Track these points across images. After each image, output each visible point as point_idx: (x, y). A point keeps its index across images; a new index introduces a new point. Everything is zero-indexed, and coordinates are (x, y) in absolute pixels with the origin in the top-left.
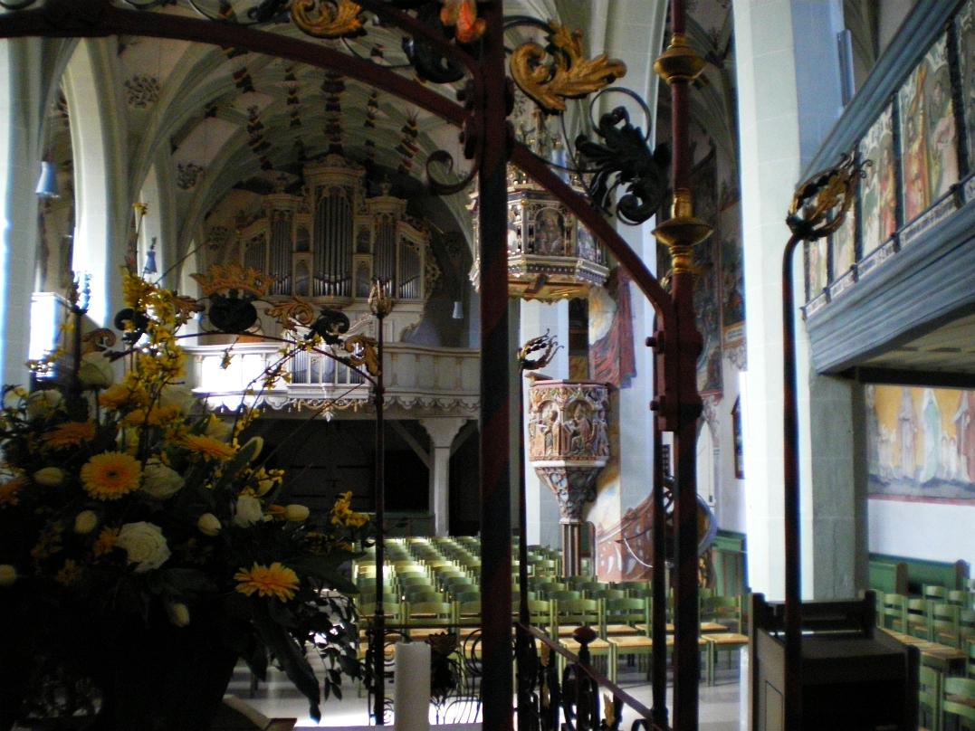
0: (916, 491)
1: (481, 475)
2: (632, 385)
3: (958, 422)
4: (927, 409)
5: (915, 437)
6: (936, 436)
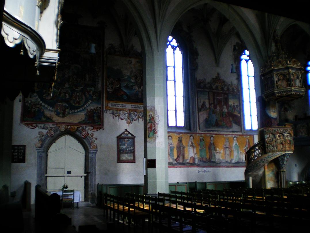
0: (231, 165)
1: (287, 152)
2: (105, 126)
3: (245, 149)
4: (235, 146)
5: (230, 152)
6: (238, 152)
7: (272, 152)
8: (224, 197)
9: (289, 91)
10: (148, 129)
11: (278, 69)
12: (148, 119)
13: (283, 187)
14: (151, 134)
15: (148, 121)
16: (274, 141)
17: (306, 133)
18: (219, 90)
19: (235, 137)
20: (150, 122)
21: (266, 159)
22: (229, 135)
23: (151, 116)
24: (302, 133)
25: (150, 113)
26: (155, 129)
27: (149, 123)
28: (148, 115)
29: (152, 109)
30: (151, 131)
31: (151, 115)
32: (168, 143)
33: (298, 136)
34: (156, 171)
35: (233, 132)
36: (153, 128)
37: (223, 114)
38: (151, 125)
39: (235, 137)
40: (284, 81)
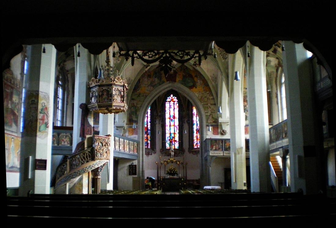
7: (100, 159)
9: (109, 106)
10: (38, 121)
13: (90, 193)
14: (43, 127)
15: (40, 110)
16: (102, 150)
17: (69, 143)
18: (8, 82)
19: (13, 138)
20: (42, 112)
21: (93, 166)
22: (10, 135)
23: (43, 105)
24: (64, 142)
25: (43, 101)
26: (47, 122)
27: (41, 113)
28: (40, 103)
29: (45, 97)
30: (42, 124)
31: (44, 104)
33: (60, 145)
34: (46, 173)
35: (12, 132)
36: (46, 121)
37: (8, 110)
38: (44, 116)
39: (13, 138)
40: (119, 96)
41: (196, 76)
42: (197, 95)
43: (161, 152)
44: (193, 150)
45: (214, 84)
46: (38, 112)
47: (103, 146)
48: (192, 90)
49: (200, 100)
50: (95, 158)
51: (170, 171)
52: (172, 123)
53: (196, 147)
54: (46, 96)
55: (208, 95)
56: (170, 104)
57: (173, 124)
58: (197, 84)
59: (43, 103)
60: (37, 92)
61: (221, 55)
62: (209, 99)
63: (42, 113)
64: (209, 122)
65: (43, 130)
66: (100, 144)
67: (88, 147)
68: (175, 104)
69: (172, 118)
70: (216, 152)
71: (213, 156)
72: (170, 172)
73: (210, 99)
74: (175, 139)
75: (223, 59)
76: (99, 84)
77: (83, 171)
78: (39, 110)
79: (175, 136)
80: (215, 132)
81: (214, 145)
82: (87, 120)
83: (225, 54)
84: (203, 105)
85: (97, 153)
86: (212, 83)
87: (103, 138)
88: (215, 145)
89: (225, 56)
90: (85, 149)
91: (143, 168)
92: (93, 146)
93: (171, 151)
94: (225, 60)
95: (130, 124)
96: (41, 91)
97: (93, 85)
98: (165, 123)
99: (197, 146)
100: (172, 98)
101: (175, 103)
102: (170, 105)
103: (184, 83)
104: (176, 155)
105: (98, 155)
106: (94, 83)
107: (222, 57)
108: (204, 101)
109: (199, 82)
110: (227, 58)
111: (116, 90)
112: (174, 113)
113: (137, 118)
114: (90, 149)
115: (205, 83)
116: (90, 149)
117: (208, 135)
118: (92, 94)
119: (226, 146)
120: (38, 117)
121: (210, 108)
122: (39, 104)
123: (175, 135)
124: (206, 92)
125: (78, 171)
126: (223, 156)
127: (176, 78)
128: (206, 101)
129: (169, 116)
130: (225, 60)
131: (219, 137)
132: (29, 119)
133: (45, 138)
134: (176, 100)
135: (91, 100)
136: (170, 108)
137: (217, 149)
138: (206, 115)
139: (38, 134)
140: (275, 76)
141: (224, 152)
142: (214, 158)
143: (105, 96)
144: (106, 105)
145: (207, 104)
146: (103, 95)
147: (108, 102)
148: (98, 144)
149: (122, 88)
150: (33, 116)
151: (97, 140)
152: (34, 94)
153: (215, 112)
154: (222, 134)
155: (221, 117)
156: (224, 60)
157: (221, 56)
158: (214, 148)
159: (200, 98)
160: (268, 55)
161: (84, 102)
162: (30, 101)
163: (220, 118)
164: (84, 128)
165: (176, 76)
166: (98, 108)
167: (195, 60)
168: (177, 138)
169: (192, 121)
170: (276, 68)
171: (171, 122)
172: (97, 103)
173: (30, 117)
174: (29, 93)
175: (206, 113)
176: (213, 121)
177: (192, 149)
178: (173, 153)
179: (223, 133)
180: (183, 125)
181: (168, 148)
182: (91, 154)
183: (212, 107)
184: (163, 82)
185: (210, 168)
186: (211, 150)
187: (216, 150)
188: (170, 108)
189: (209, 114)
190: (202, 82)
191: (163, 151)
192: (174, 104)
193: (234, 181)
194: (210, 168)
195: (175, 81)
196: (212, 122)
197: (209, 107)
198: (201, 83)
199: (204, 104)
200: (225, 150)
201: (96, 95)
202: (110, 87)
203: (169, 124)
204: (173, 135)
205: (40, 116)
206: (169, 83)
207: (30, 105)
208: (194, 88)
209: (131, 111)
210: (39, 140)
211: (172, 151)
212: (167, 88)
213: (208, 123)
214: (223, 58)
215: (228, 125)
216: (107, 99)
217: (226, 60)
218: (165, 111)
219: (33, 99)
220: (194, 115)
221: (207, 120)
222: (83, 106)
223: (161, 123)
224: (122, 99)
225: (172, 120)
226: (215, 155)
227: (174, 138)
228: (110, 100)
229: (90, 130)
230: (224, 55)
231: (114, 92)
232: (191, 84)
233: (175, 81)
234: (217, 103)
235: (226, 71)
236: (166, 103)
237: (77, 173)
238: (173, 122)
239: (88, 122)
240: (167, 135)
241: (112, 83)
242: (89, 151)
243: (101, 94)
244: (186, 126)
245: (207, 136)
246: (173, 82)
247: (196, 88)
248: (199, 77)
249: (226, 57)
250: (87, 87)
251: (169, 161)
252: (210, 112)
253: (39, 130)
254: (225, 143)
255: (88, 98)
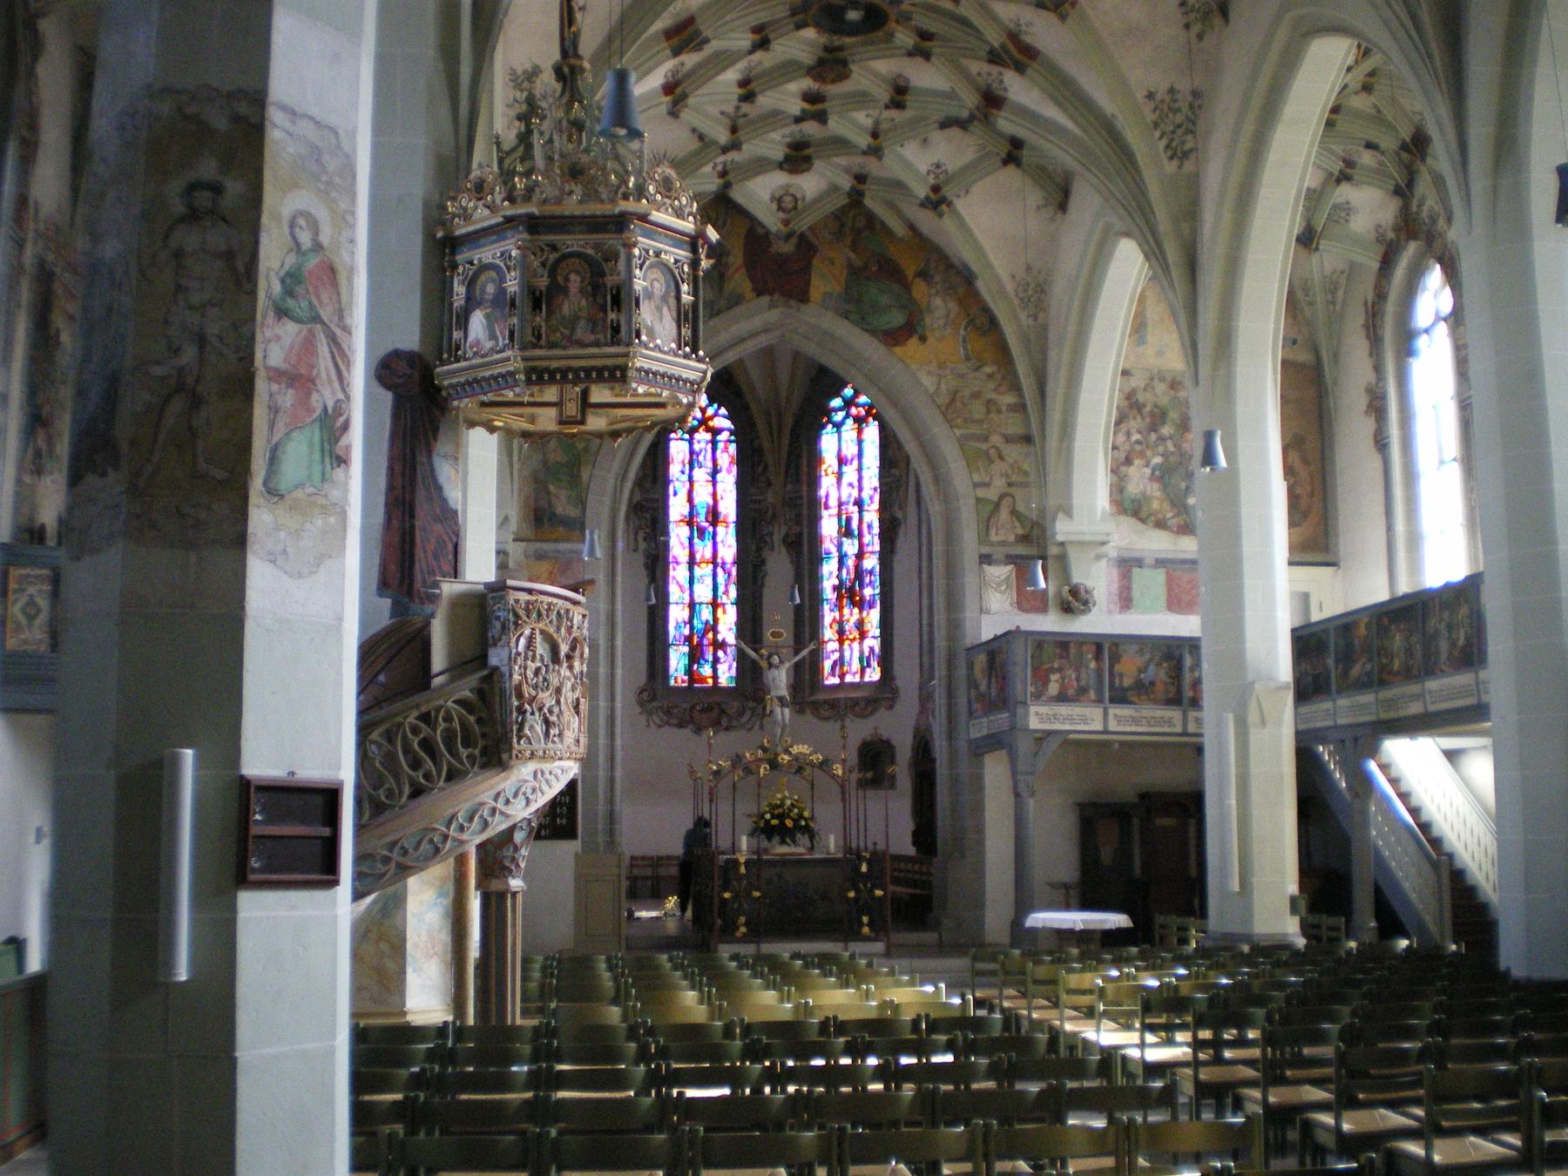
7: (544, 758)
8: (633, 986)
10: (262, 386)
11: (458, 50)
12: (276, 265)
15: (277, 288)
20: (290, 303)
21: (500, 805)
23: (305, 239)
27: (282, 313)
28: (277, 217)
32: (1195, 703)
38: (309, 345)
41: (923, 275)
42: (928, 382)
43: (641, 704)
44: (820, 697)
45: (1031, 321)
46: (253, 293)
47: (555, 658)
48: (897, 350)
49: (944, 414)
50: (510, 749)
51: (773, 817)
52: (704, 549)
53: (836, 681)
54: (326, 158)
55: (992, 385)
56: (691, 442)
57: (708, 555)
58: (928, 320)
59: (301, 213)
60: (243, 109)
61: (1157, 134)
62: (993, 408)
63: (298, 321)
64: (994, 538)
65: (301, 485)
66: (541, 648)
67: (458, 668)
68: (721, 446)
69: (701, 519)
70: (1064, 710)
71: (1050, 733)
72: (775, 822)
73: (1004, 408)
74: (716, 632)
75: (1171, 158)
76: (535, 210)
77: (425, 846)
78: (269, 284)
79: (716, 620)
80: (1030, 601)
81: (1051, 670)
82: (433, 470)
83: (1179, 126)
84: (962, 442)
85: (521, 711)
86: (1015, 316)
87: (560, 602)
88: (1060, 670)
89: (1183, 143)
90: (437, 681)
91: (611, 801)
92: (493, 660)
93: (776, 701)
94: (1180, 167)
95: (537, 540)
96: (286, 100)
97: (482, 217)
98: (666, 546)
99: (842, 676)
100: (703, 411)
101: (719, 438)
102: (692, 452)
103: (854, 307)
104: (724, 722)
105: (532, 728)
106: (491, 207)
107: (1163, 143)
108: (966, 420)
109: (940, 309)
110: (1191, 150)
111: (651, 266)
112: (714, 495)
113: (582, 503)
114: (473, 680)
115: (985, 324)
116: (473, 680)
117: (988, 612)
118: (471, 284)
119: (1121, 675)
120: (259, 355)
121: (1001, 458)
122: (265, 219)
123: (720, 610)
124: (977, 369)
125: (395, 843)
126: (1185, 734)
127: (808, 283)
128: (977, 417)
129: (686, 511)
130: (1180, 167)
131: (1050, 622)
132: (157, 371)
133: (319, 560)
134: (722, 422)
135: (464, 323)
136: (691, 469)
137: (1071, 692)
138: (978, 500)
139: (261, 517)
140: (1366, 290)
141: (1111, 711)
142: (1054, 744)
143: (574, 302)
144: (583, 363)
145: (986, 439)
146: (557, 289)
147: (597, 344)
148: (531, 640)
149: (683, 254)
150: (202, 340)
151: (522, 613)
152: (221, 123)
153: (1025, 485)
154: (1067, 609)
155: (1069, 513)
156: (1175, 162)
157: (1161, 137)
158: (1053, 689)
159: (943, 400)
160: (1349, 171)
161: (409, 338)
162: (175, 187)
163: (1060, 516)
164: (413, 527)
165: (807, 269)
166: (529, 382)
167: (937, 177)
168: (727, 628)
169: (816, 539)
170: (1382, 249)
171: (696, 540)
172: (523, 348)
173: (177, 351)
174: (165, 108)
175: (976, 485)
176: (1020, 531)
177: (812, 694)
178: (787, 711)
179: (1074, 601)
180: (763, 562)
181: (680, 684)
182: (479, 721)
183: (1013, 452)
184: (737, 300)
185: (1031, 802)
186: (1037, 696)
187: (1062, 698)
188: (691, 469)
189: (992, 494)
190: (953, 306)
191: (653, 698)
192: (714, 443)
193: (1237, 889)
194: (1031, 802)
195: (803, 297)
196: (1012, 538)
197: (992, 451)
198: (952, 316)
199: (966, 438)
200: (1112, 701)
201: (501, 291)
202: (611, 240)
203: (687, 552)
204: (706, 614)
205: (275, 345)
206: (771, 306)
207: (171, 229)
208: (913, 342)
209: (545, 462)
210: (266, 587)
211: (781, 699)
212: (753, 335)
213: (992, 544)
214: (1170, 153)
215: (1099, 557)
216: (594, 324)
217: (1189, 166)
218: (666, 482)
219: (208, 169)
220: (827, 507)
221: (986, 525)
222: (402, 367)
223: (642, 545)
224: (686, 332)
225: (702, 533)
226: (1057, 727)
227: (713, 627)
228: (616, 330)
229: (450, 547)
230: (1180, 132)
231: (637, 272)
232: (897, 319)
233: (803, 297)
234: (1043, 437)
235: (1185, 227)
236: (673, 435)
237: (387, 860)
238: (709, 544)
239: (439, 488)
240: (677, 614)
241: (629, 206)
242: (467, 694)
243: (543, 282)
244: (778, 565)
245: (985, 619)
246: (793, 303)
247: (923, 339)
248: (937, 279)
249: (1188, 146)
250: (429, 236)
251: (786, 757)
252: (999, 484)
253: (265, 484)
254: (1115, 658)
255: (443, 320)
